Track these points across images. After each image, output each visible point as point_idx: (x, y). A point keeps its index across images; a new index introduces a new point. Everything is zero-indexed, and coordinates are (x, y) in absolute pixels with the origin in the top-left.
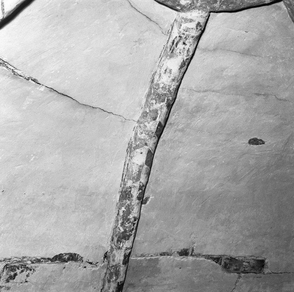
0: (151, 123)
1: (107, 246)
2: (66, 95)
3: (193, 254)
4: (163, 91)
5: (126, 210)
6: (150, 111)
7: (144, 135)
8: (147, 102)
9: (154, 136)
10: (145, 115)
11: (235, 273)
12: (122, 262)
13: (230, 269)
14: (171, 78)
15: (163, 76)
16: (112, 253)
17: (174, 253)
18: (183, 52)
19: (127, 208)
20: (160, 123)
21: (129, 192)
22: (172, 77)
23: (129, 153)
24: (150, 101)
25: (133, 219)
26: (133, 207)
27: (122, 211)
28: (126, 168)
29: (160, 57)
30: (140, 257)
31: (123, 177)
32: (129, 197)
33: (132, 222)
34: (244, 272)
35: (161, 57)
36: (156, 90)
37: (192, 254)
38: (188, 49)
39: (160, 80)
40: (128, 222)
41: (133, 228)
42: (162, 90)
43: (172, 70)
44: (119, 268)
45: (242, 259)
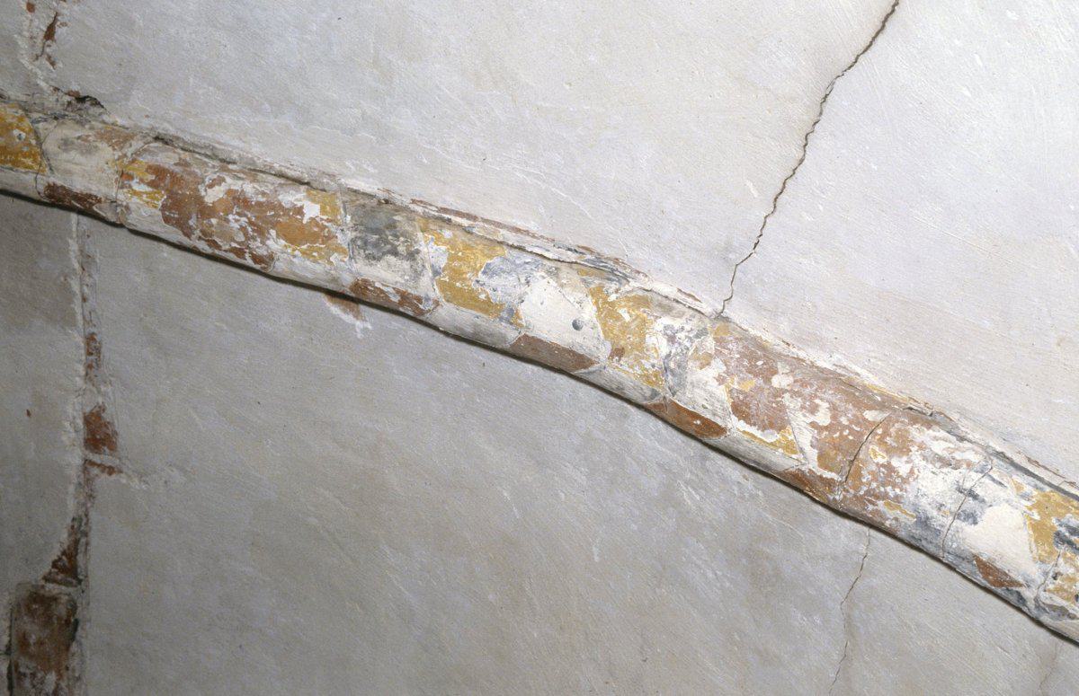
0: (721, 392)
1: (135, 109)
2: (883, 26)
3: (95, 471)
4: (874, 468)
5: (304, 222)
6: (779, 393)
7: (664, 348)
8: (816, 377)
9: (655, 394)
10: (760, 363)
11: (10, 636)
12: (59, 183)
13: (25, 618)
14: (934, 513)
15: (946, 478)
16: (101, 136)
17: (99, 392)
18: (1059, 590)
19: (316, 229)
20: (721, 431)
21: (389, 247)
22: (938, 519)
23: (572, 257)
24: (826, 396)
25: (262, 252)
26: (321, 257)
27: (299, 204)
28: (503, 234)
29: (1029, 460)
30: (81, 251)
31: (458, 213)
32: (366, 243)
33: (248, 247)
34: (14, 675)
35: (1031, 468)
36: (877, 434)
37: (93, 464)
38: (1071, 611)
39: (925, 458)
40: (250, 229)
41: (219, 247)
42: (877, 464)
43: (975, 523)
44: (31, 167)
45: (70, 668)
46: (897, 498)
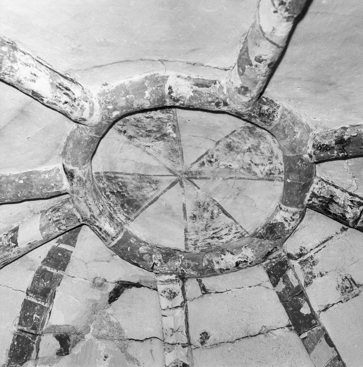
46: (13, 76)
